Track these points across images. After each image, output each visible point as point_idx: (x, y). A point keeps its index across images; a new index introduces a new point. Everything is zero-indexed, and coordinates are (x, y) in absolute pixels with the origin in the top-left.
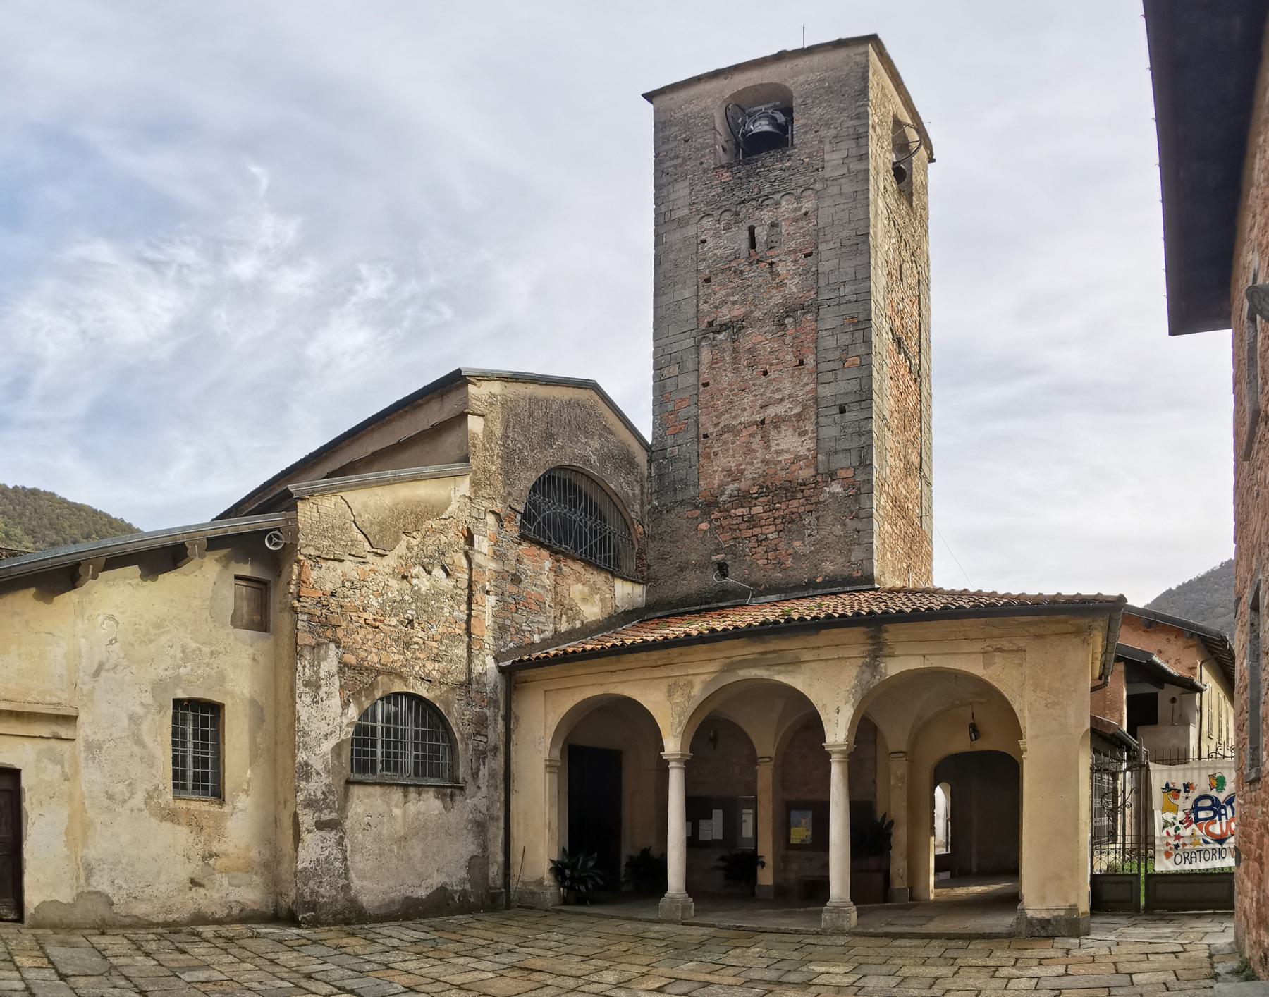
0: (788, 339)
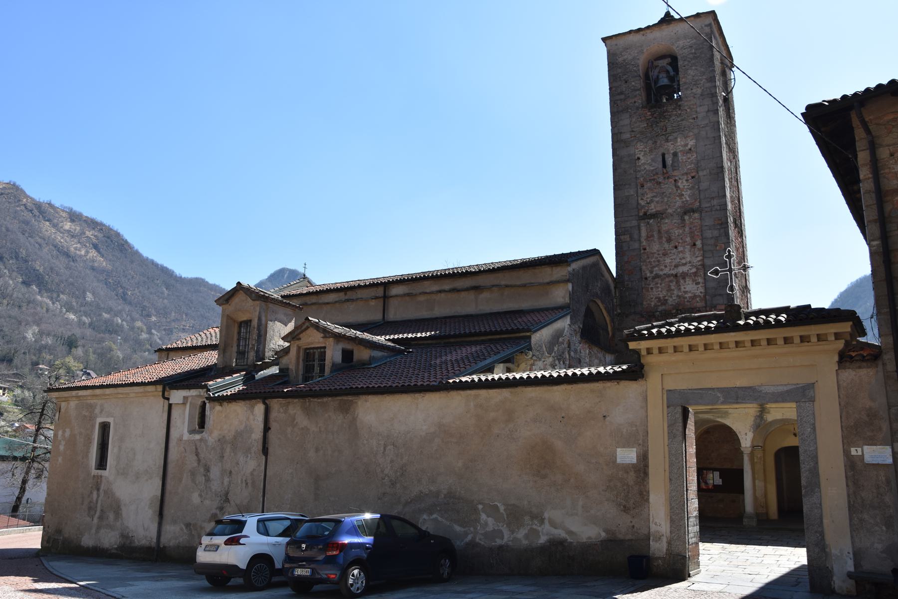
0: (687, 229)
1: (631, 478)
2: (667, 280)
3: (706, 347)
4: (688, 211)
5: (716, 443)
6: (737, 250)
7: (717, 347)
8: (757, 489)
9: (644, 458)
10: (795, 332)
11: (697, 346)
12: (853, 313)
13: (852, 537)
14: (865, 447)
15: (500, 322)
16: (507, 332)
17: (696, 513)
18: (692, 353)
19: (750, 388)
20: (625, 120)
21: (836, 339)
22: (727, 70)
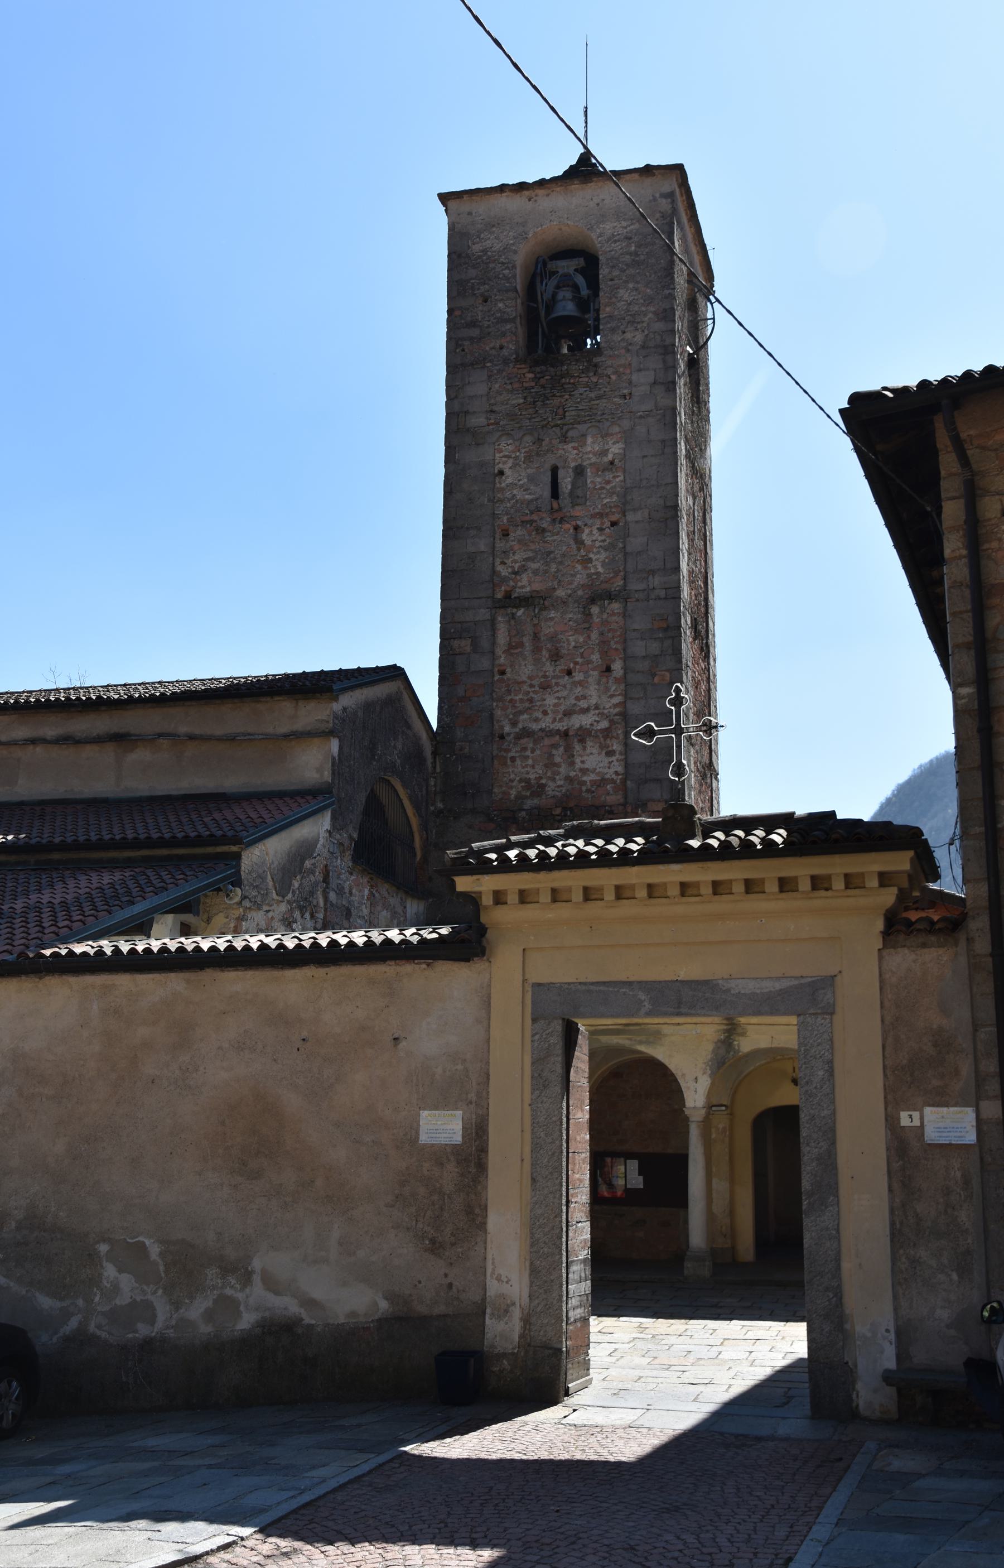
0: (595, 635)
1: (449, 1176)
2: (547, 742)
3: (621, 893)
4: (598, 595)
5: (634, 1098)
6: (697, 686)
7: (642, 893)
8: (715, 1198)
9: (478, 1132)
10: (802, 868)
11: (600, 889)
12: (917, 832)
13: (895, 1297)
14: (928, 1110)
15: (172, 818)
16: (187, 842)
17: (584, 1254)
18: (591, 904)
19: (706, 982)
20: (478, 386)
21: (882, 885)
22: (700, 299)
